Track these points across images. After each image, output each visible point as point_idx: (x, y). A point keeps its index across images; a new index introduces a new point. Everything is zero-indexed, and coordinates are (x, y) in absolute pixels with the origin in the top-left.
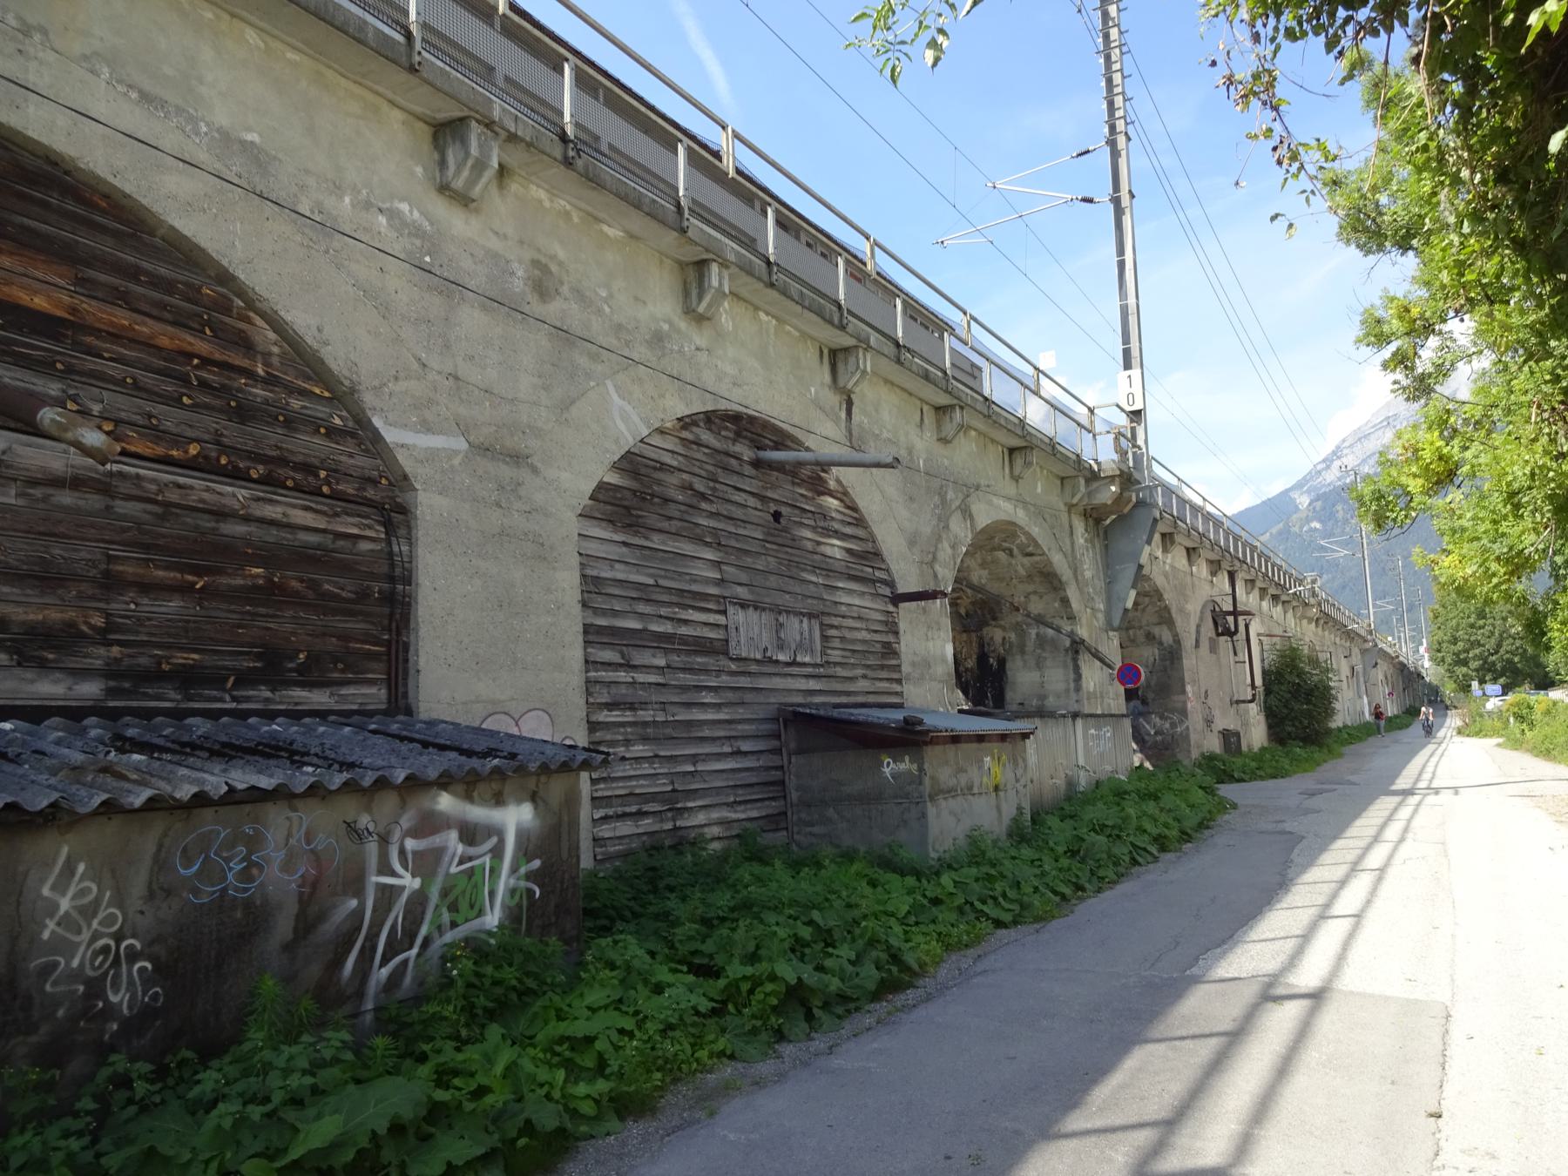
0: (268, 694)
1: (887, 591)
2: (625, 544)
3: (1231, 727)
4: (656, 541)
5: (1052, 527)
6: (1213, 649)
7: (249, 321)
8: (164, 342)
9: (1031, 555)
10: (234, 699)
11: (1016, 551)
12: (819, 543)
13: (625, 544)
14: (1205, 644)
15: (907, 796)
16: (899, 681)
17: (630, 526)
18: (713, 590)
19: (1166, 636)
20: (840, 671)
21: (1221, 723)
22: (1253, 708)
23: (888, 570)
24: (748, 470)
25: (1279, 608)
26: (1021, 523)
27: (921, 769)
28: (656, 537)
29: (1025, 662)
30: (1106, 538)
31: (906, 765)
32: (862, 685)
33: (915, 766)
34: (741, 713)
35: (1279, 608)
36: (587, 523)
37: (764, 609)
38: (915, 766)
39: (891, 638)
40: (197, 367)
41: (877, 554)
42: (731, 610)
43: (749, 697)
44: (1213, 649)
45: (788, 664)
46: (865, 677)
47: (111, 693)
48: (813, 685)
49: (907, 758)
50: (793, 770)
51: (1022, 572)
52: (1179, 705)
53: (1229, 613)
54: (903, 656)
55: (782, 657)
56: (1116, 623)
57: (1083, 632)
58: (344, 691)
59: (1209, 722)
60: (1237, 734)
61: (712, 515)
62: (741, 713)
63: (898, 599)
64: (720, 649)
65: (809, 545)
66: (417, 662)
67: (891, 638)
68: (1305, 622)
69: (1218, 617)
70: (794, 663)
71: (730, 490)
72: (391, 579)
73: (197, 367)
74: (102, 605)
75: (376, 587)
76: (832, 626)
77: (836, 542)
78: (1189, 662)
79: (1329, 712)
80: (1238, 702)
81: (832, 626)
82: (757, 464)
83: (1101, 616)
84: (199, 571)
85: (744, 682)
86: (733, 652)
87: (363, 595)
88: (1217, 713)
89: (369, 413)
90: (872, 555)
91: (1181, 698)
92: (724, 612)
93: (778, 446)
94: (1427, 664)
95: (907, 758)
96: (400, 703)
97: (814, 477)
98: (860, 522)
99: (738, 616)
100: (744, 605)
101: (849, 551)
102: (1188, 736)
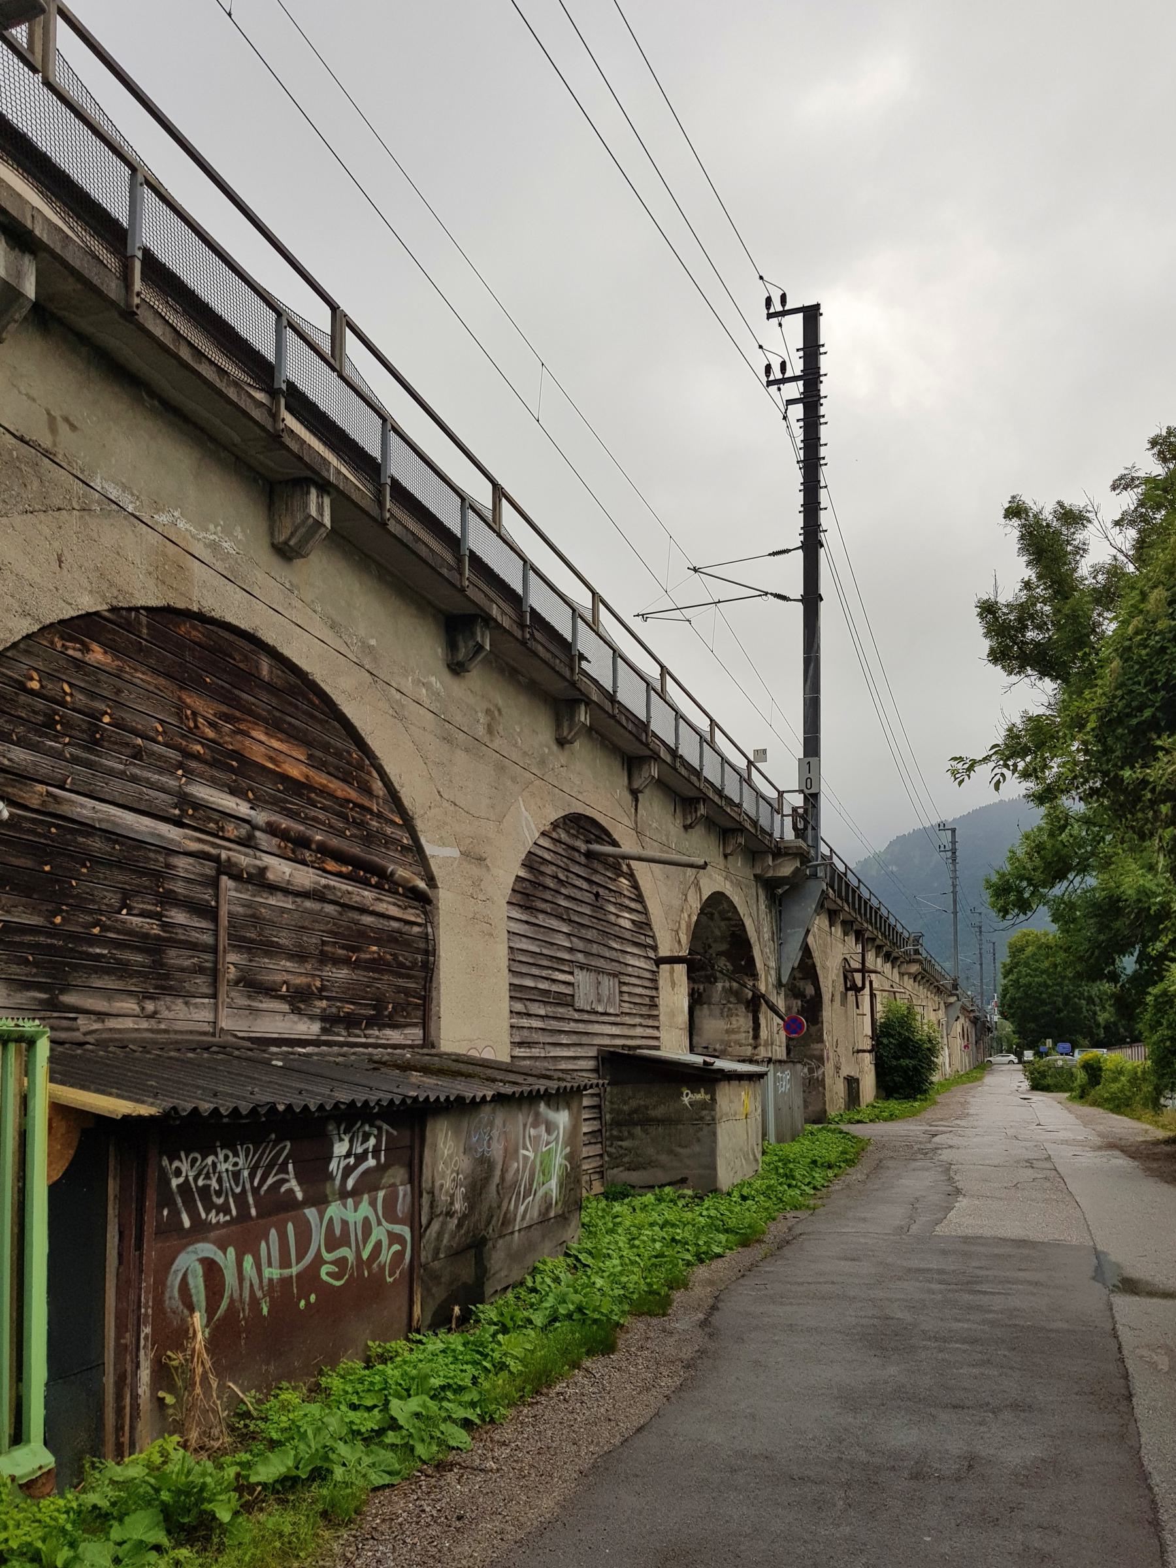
0: (377, 1033)
1: (652, 954)
2: (527, 922)
3: (852, 1074)
4: (541, 920)
5: (746, 896)
6: (844, 1002)
7: (369, 774)
8: (339, 793)
9: (729, 919)
10: (365, 1036)
11: (716, 915)
12: (618, 916)
13: (527, 922)
14: (838, 998)
15: (702, 1118)
16: (657, 1028)
17: (527, 908)
18: (567, 956)
19: (810, 990)
20: (627, 1020)
21: (846, 1071)
22: (868, 1058)
23: (653, 937)
24: (583, 860)
25: (889, 965)
26: (728, 893)
27: (713, 1099)
28: (541, 916)
29: (710, 1010)
30: (780, 905)
31: (701, 1096)
32: (639, 1031)
33: (708, 1097)
34: (579, 1052)
35: (889, 965)
36: (510, 907)
37: (591, 971)
38: (708, 1097)
39: (654, 993)
40: (352, 809)
41: (648, 925)
42: (576, 971)
43: (585, 1040)
44: (844, 1002)
45: (602, 1014)
46: (641, 1025)
47: (324, 1030)
48: (615, 1030)
49: (702, 1090)
50: (608, 1097)
51: (717, 933)
52: (817, 1053)
53: (857, 971)
54: (661, 1008)
55: (600, 1010)
56: (784, 980)
57: (762, 988)
58: (407, 1031)
59: (838, 1069)
60: (857, 1081)
61: (568, 897)
62: (579, 1052)
63: (659, 961)
64: (566, 1001)
65: (612, 918)
66: (439, 1011)
67: (654, 993)
68: (906, 977)
69: (847, 973)
70: (605, 1014)
71: (574, 877)
72: (426, 952)
73: (352, 809)
74: (319, 973)
75: (419, 958)
76: (624, 983)
77: (627, 915)
78: (827, 1014)
79: (932, 1067)
80: (859, 1051)
81: (624, 983)
82: (589, 855)
83: (773, 972)
84: (354, 949)
85: (581, 1027)
86: (577, 1005)
87: (415, 963)
88: (843, 1060)
89: (419, 834)
90: (644, 926)
91: (819, 1046)
92: (572, 973)
93: (600, 840)
94: (996, 1018)
95: (702, 1090)
96: (428, 1042)
97: (617, 865)
98: (640, 898)
99: (581, 977)
100: (582, 967)
101: (633, 921)
102: (823, 1080)
